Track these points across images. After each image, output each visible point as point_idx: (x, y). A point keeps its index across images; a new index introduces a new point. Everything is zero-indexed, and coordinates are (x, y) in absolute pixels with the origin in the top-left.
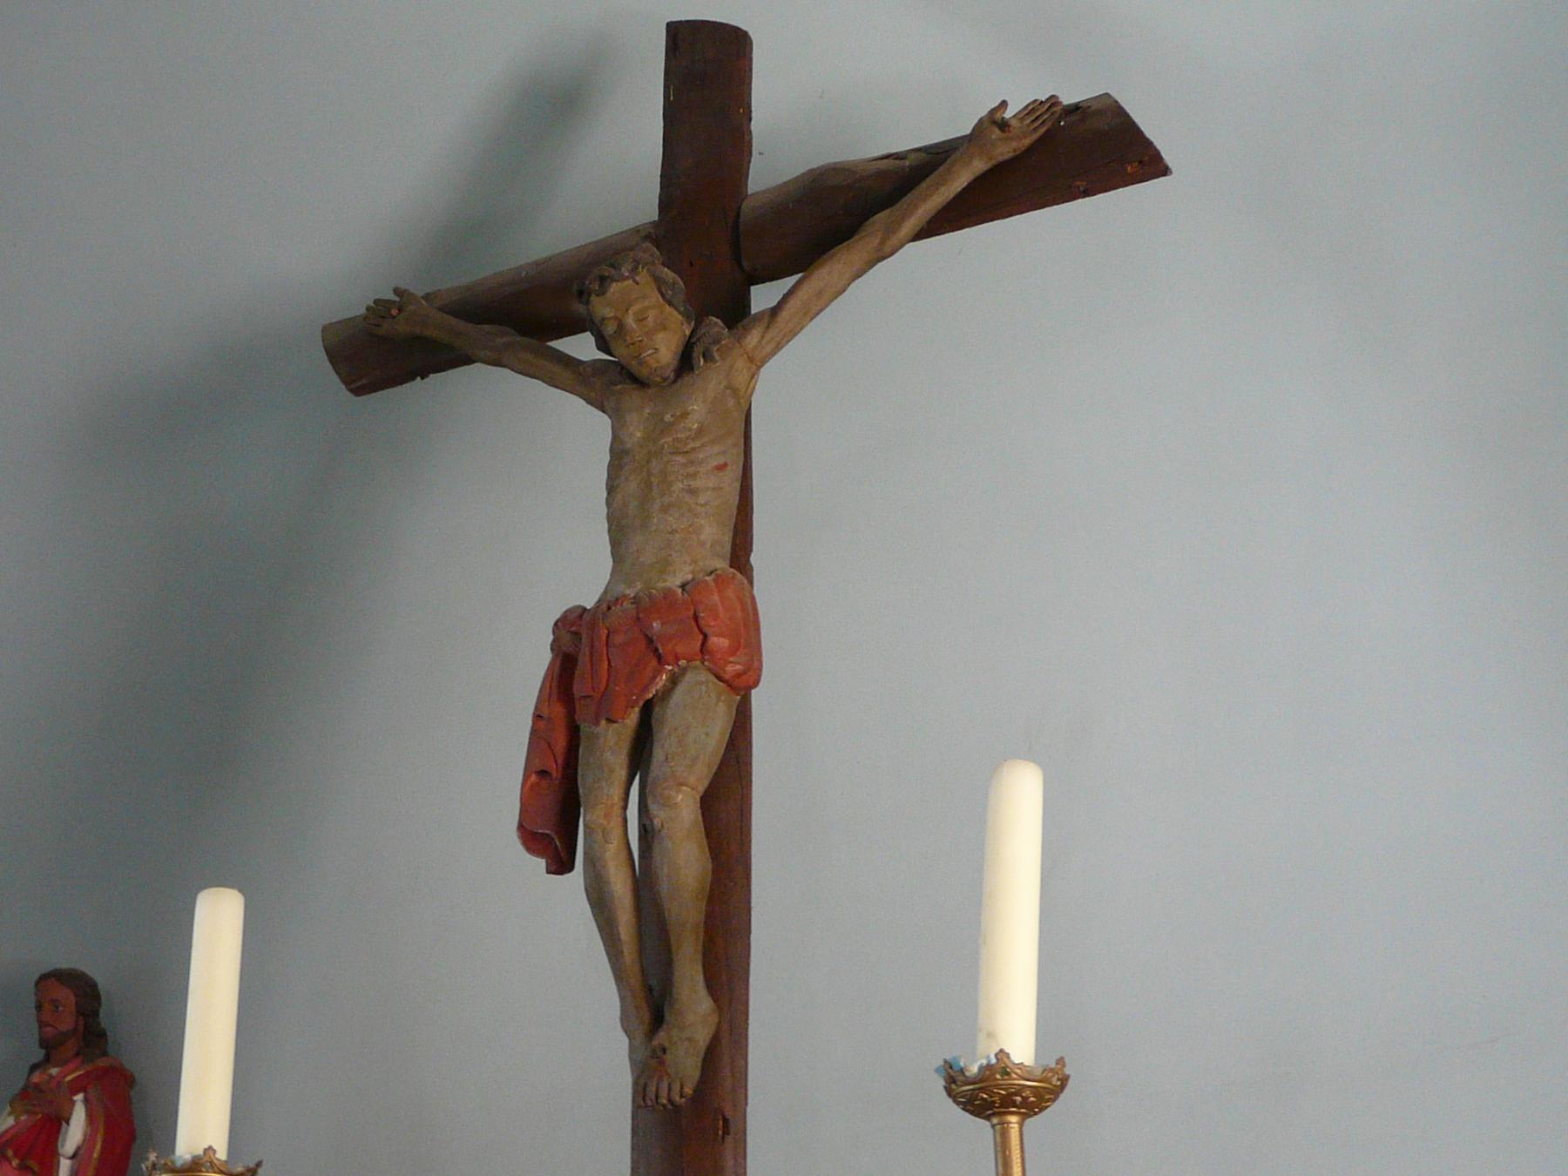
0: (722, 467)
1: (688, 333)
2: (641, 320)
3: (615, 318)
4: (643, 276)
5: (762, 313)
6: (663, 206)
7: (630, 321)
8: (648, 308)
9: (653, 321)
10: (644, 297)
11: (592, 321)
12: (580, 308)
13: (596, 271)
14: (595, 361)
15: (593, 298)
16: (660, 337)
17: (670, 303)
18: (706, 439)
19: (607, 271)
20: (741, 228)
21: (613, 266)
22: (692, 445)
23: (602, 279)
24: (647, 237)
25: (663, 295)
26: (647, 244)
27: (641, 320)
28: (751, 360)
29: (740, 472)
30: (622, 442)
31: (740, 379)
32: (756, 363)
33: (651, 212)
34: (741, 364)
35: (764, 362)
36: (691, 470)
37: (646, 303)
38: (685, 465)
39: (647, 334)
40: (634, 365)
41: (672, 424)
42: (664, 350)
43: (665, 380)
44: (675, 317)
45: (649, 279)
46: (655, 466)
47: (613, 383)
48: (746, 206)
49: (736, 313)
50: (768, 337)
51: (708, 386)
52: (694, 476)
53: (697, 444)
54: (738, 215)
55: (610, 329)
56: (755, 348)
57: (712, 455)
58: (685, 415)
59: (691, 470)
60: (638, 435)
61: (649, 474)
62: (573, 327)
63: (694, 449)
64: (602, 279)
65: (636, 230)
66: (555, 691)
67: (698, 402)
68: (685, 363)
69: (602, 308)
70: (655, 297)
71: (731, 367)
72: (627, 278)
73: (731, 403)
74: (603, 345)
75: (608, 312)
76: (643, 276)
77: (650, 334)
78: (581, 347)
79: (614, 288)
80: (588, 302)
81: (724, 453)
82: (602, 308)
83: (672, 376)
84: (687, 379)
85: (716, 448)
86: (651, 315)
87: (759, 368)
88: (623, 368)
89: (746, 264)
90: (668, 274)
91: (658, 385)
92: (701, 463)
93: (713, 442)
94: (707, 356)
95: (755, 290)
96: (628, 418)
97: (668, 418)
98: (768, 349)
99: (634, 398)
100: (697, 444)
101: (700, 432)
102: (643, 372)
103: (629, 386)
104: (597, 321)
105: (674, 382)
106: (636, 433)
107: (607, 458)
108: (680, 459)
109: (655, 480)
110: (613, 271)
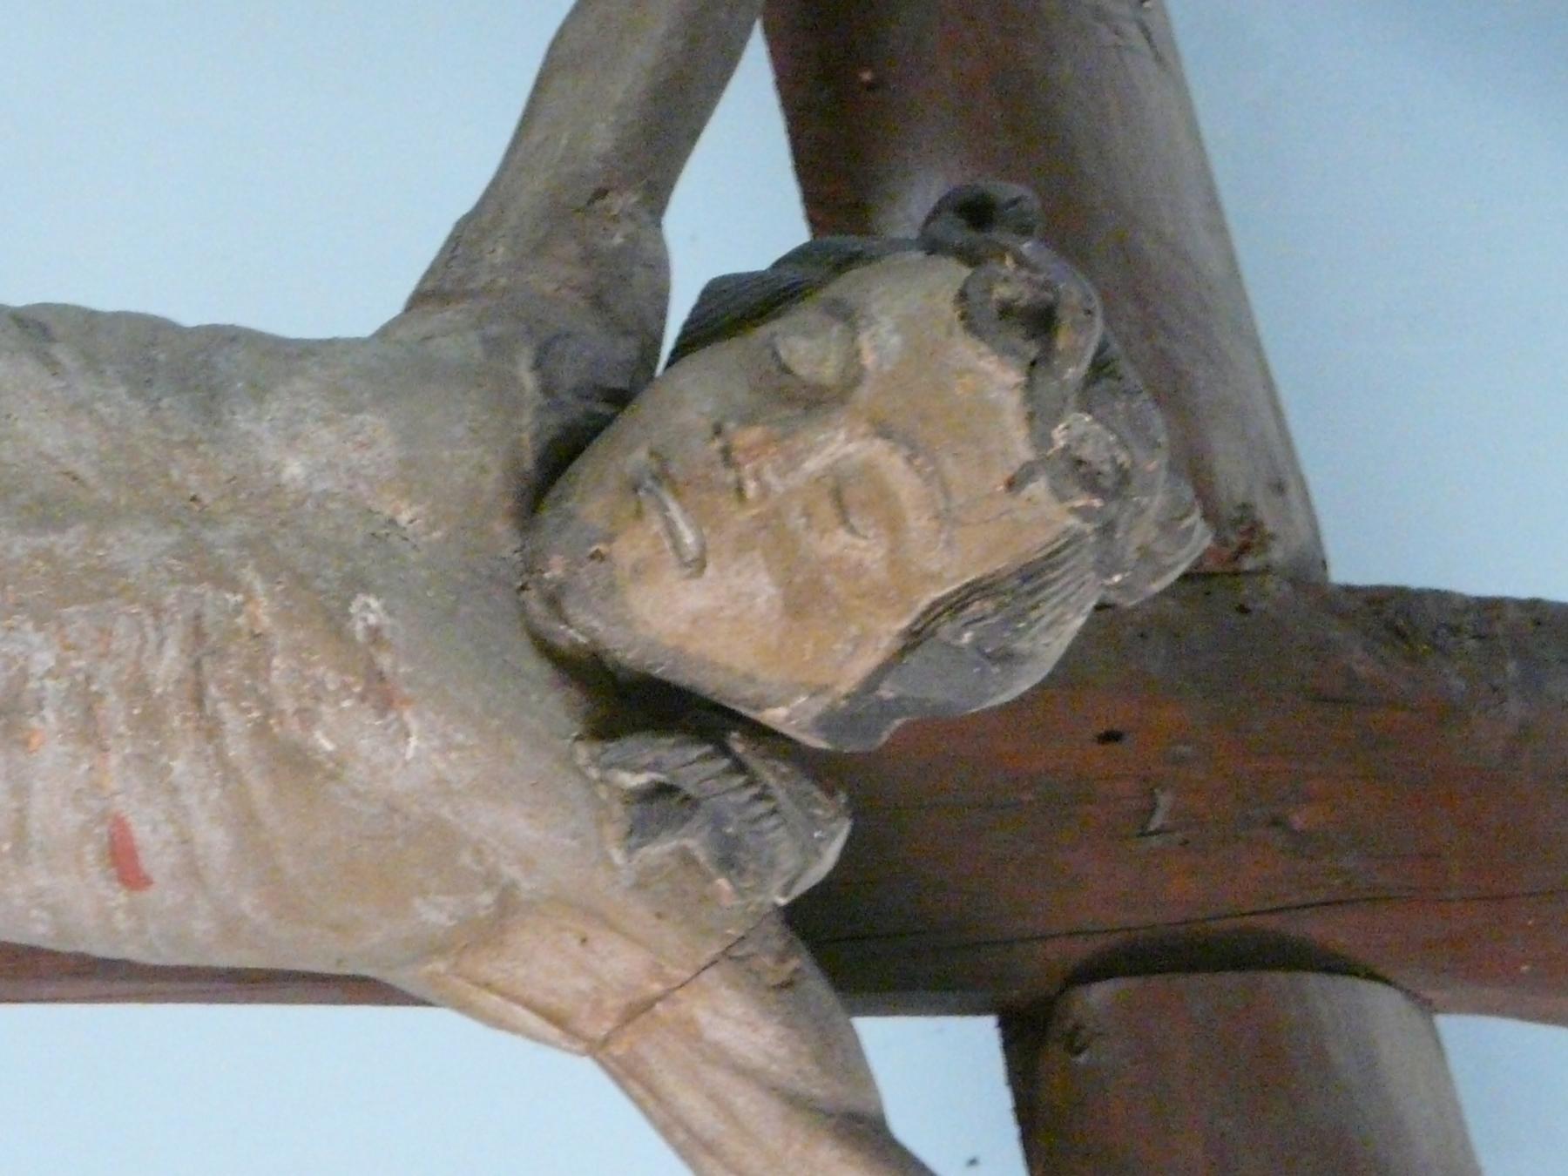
0: (124, 862)
1: (774, 716)
2: (841, 496)
3: (853, 377)
4: (1048, 513)
5: (850, 1063)
6: (1398, 616)
7: (837, 445)
8: (894, 525)
9: (865, 537)
10: (944, 518)
11: (846, 262)
12: (916, 198)
13: (1073, 290)
14: (659, 266)
15: (954, 273)
16: (759, 587)
17: (915, 638)
18: (260, 791)
19: (1077, 344)
20: (1278, 979)
21: (1101, 367)
22: (235, 722)
23: (1040, 321)
24: (1243, 534)
25: (955, 605)
26: (1201, 538)
27: (841, 496)
28: (638, 1011)
29: (100, 949)
30: (259, 392)
31: (544, 961)
32: (619, 1038)
33: (1355, 563)
34: (621, 965)
35: (629, 1075)
36: (115, 711)
37: (918, 523)
38: (139, 688)
39: (771, 523)
40: (625, 453)
41: (336, 624)
42: (689, 606)
43: (553, 601)
44: (852, 657)
45: (1035, 542)
46: (138, 547)
47: (563, 359)
48: (1382, 1006)
49: (860, 945)
50: (745, 1100)
51: (520, 804)
52: (88, 730)
53: (237, 748)
54: (1372, 976)
55: (804, 345)
56: (689, 1031)
57: (186, 814)
58: (382, 695)
59: (115, 711)
60: (294, 469)
61: (104, 516)
62: (837, 165)
63: (212, 730)
64: (1040, 321)
65: (1283, 481)
66: (1114, 939)
67: (451, 761)
68: (632, 702)
69: (905, 310)
70: (948, 566)
71: (595, 915)
72: (1042, 440)
73: (435, 913)
74: (735, 310)
75: (881, 343)
76: (1048, 513)
77: (773, 536)
78: (735, 201)
79: (995, 376)
80: (933, 247)
81: (192, 871)
82: (905, 310)
83: (571, 635)
84: (554, 708)
85: (214, 839)
86: (863, 548)
87: (596, 1049)
88: (621, 399)
89: (1099, 995)
90: (1051, 637)
91: (531, 566)
92: (148, 763)
93: (245, 821)
94: (662, 803)
95: (973, 1042)
96: (372, 422)
97: (368, 611)
98: (690, 1102)
99: (478, 450)
100: (237, 748)
101: (293, 763)
102: (590, 497)
103: (528, 430)
104: (843, 287)
105: (546, 649)
106: (301, 454)
107: (190, 314)
108: (168, 665)
109: (67, 542)
110: (1074, 373)
